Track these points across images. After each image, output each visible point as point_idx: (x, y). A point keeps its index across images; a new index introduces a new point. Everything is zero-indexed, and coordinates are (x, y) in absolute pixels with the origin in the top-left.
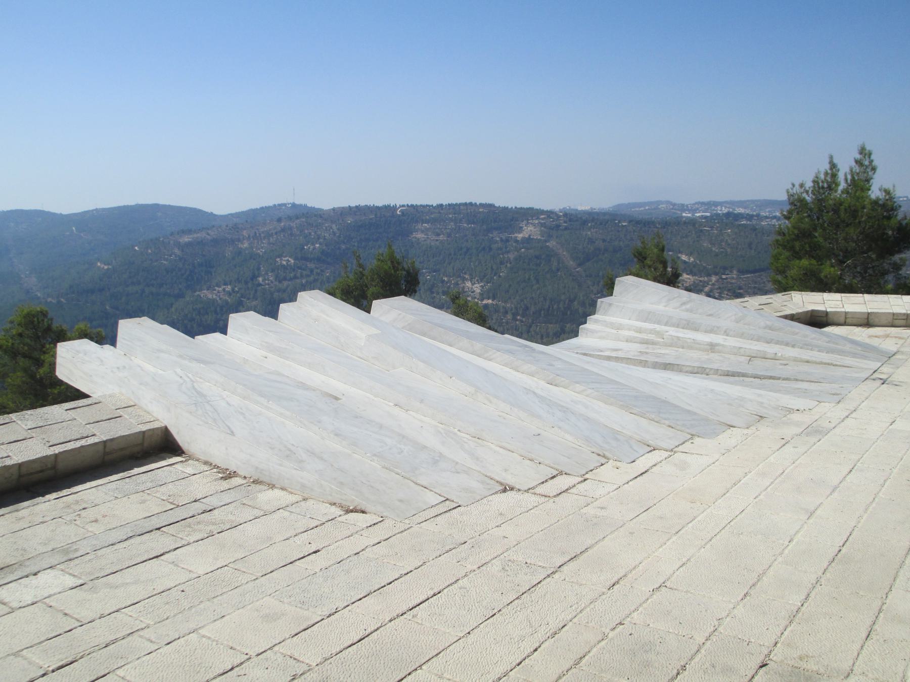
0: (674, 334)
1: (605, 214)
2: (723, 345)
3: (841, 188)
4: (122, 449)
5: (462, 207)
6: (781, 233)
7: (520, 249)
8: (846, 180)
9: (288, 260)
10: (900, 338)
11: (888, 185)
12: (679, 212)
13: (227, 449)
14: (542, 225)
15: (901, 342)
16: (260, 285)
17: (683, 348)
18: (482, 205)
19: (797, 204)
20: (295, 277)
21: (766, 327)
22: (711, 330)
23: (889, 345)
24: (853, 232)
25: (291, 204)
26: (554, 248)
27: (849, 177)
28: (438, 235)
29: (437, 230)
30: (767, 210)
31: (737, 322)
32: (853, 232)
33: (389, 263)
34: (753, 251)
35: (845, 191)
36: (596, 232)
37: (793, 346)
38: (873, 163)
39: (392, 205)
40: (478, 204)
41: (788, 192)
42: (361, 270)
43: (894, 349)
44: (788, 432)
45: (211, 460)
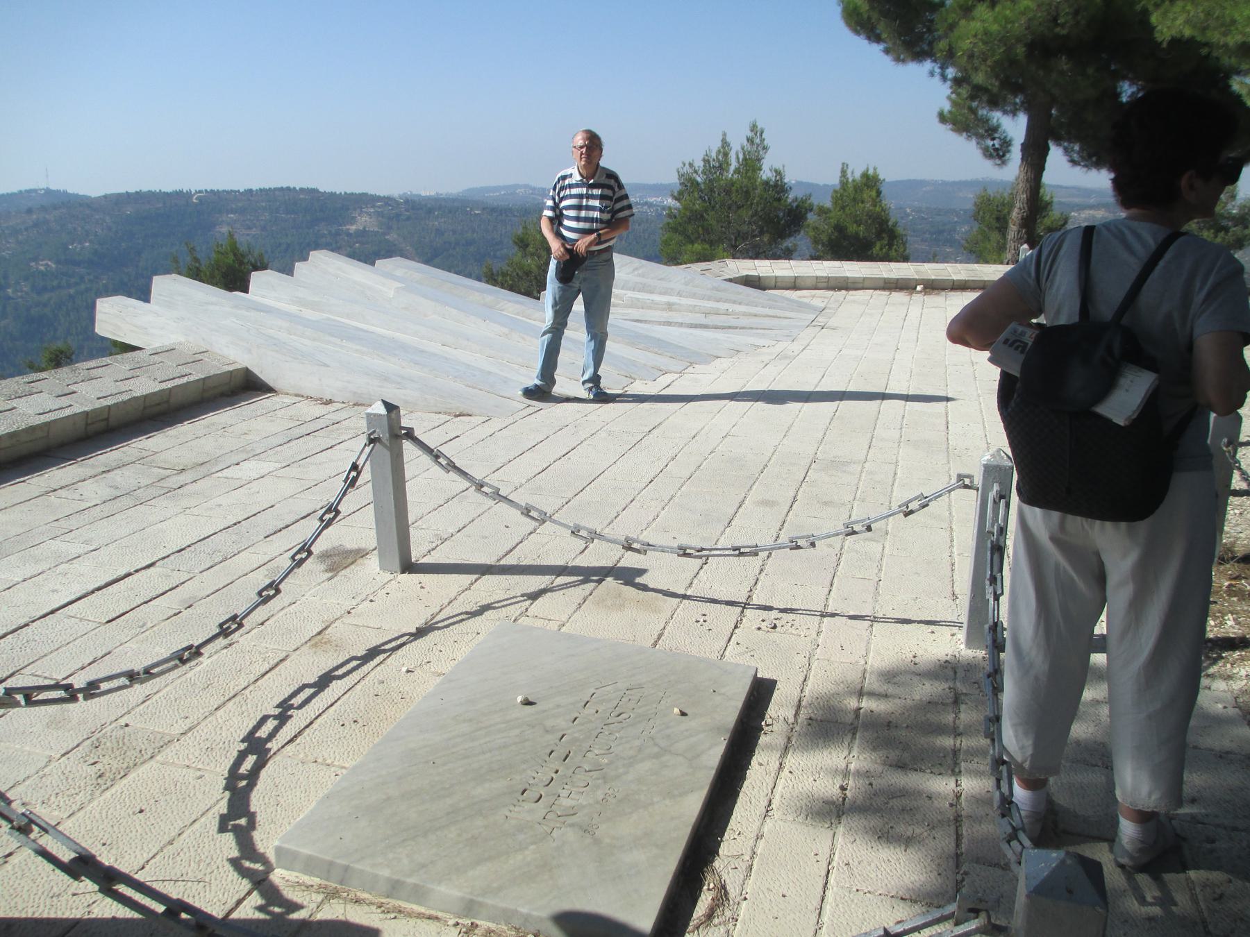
0: (632, 296)
1: (454, 200)
2: (679, 304)
3: (732, 168)
4: (215, 387)
5: (277, 193)
6: (671, 216)
7: (354, 244)
8: (738, 158)
9: (47, 264)
10: (825, 298)
11: (778, 166)
12: (540, 198)
13: (320, 380)
14: (379, 214)
15: (826, 301)
16: (10, 298)
17: (642, 308)
18: (302, 190)
19: (688, 186)
20: (59, 287)
21: (714, 289)
22: (666, 292)
23: (818, 303)
24: (746, 214)
25: (43, 189)
26: (396, 242)
27: (741, 156)
28: (250, 228)
29: (247, 222)
30: (637, 195)
31: (687, 285)
32: (746, 214)
33: (232, 257)
34: (624, 242)
35: (737, 171)
36: (445, 222)
37: (740, 304)
38: (765, 142)
39: (185, 191)
40: (298, 188)
41: (678, 172)
42: (197, 265)
43: (822, 305)
44: (766, 359)
45: (302, 393)
